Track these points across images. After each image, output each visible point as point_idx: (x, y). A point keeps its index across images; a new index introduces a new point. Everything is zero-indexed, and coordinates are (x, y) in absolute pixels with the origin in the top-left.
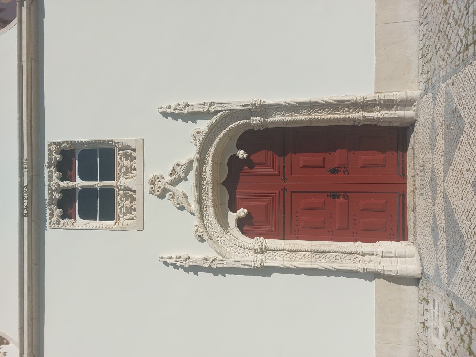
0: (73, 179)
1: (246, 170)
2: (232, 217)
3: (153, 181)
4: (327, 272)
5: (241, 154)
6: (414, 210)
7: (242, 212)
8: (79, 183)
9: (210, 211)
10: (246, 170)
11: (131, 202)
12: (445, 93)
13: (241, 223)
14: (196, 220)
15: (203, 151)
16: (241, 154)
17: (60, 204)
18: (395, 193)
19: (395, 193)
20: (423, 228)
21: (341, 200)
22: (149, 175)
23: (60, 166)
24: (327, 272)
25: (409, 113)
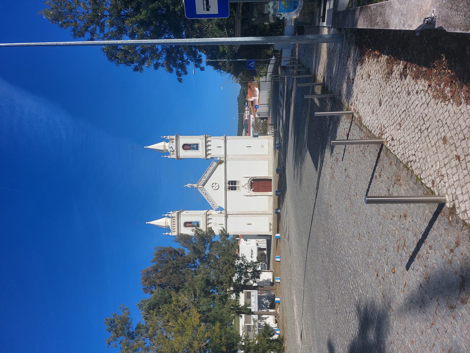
0: (230, 185)
1: (253, 184)
2: (252, 190)
3: (242, 185)
4: (263, 195)
5: (253, 182)
6: (256, 177)
7: (253, 189)
8: (231, 186)
9: (249, 189)
10: (253, 184)
11: (422, 179)
12: (348, 78)
13: (253, 190)
14: (248, 190)
15: (248, 182)
16: (253, 182)
17: (228, 188)
18: (412, 259)
19: (412, 259)
20: (328, 252)
21: (265, 187)
22: (241, 185)
23: (228, 183)
24: (263, 195)
25: (271, 178)
